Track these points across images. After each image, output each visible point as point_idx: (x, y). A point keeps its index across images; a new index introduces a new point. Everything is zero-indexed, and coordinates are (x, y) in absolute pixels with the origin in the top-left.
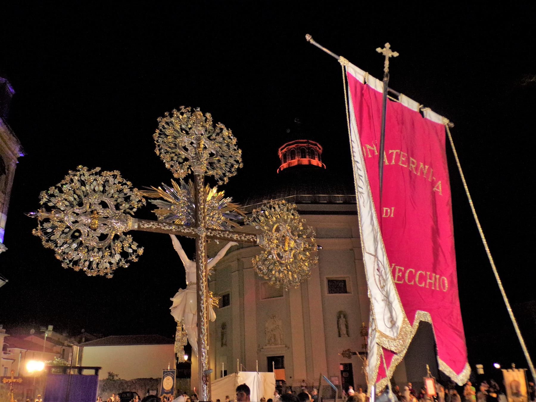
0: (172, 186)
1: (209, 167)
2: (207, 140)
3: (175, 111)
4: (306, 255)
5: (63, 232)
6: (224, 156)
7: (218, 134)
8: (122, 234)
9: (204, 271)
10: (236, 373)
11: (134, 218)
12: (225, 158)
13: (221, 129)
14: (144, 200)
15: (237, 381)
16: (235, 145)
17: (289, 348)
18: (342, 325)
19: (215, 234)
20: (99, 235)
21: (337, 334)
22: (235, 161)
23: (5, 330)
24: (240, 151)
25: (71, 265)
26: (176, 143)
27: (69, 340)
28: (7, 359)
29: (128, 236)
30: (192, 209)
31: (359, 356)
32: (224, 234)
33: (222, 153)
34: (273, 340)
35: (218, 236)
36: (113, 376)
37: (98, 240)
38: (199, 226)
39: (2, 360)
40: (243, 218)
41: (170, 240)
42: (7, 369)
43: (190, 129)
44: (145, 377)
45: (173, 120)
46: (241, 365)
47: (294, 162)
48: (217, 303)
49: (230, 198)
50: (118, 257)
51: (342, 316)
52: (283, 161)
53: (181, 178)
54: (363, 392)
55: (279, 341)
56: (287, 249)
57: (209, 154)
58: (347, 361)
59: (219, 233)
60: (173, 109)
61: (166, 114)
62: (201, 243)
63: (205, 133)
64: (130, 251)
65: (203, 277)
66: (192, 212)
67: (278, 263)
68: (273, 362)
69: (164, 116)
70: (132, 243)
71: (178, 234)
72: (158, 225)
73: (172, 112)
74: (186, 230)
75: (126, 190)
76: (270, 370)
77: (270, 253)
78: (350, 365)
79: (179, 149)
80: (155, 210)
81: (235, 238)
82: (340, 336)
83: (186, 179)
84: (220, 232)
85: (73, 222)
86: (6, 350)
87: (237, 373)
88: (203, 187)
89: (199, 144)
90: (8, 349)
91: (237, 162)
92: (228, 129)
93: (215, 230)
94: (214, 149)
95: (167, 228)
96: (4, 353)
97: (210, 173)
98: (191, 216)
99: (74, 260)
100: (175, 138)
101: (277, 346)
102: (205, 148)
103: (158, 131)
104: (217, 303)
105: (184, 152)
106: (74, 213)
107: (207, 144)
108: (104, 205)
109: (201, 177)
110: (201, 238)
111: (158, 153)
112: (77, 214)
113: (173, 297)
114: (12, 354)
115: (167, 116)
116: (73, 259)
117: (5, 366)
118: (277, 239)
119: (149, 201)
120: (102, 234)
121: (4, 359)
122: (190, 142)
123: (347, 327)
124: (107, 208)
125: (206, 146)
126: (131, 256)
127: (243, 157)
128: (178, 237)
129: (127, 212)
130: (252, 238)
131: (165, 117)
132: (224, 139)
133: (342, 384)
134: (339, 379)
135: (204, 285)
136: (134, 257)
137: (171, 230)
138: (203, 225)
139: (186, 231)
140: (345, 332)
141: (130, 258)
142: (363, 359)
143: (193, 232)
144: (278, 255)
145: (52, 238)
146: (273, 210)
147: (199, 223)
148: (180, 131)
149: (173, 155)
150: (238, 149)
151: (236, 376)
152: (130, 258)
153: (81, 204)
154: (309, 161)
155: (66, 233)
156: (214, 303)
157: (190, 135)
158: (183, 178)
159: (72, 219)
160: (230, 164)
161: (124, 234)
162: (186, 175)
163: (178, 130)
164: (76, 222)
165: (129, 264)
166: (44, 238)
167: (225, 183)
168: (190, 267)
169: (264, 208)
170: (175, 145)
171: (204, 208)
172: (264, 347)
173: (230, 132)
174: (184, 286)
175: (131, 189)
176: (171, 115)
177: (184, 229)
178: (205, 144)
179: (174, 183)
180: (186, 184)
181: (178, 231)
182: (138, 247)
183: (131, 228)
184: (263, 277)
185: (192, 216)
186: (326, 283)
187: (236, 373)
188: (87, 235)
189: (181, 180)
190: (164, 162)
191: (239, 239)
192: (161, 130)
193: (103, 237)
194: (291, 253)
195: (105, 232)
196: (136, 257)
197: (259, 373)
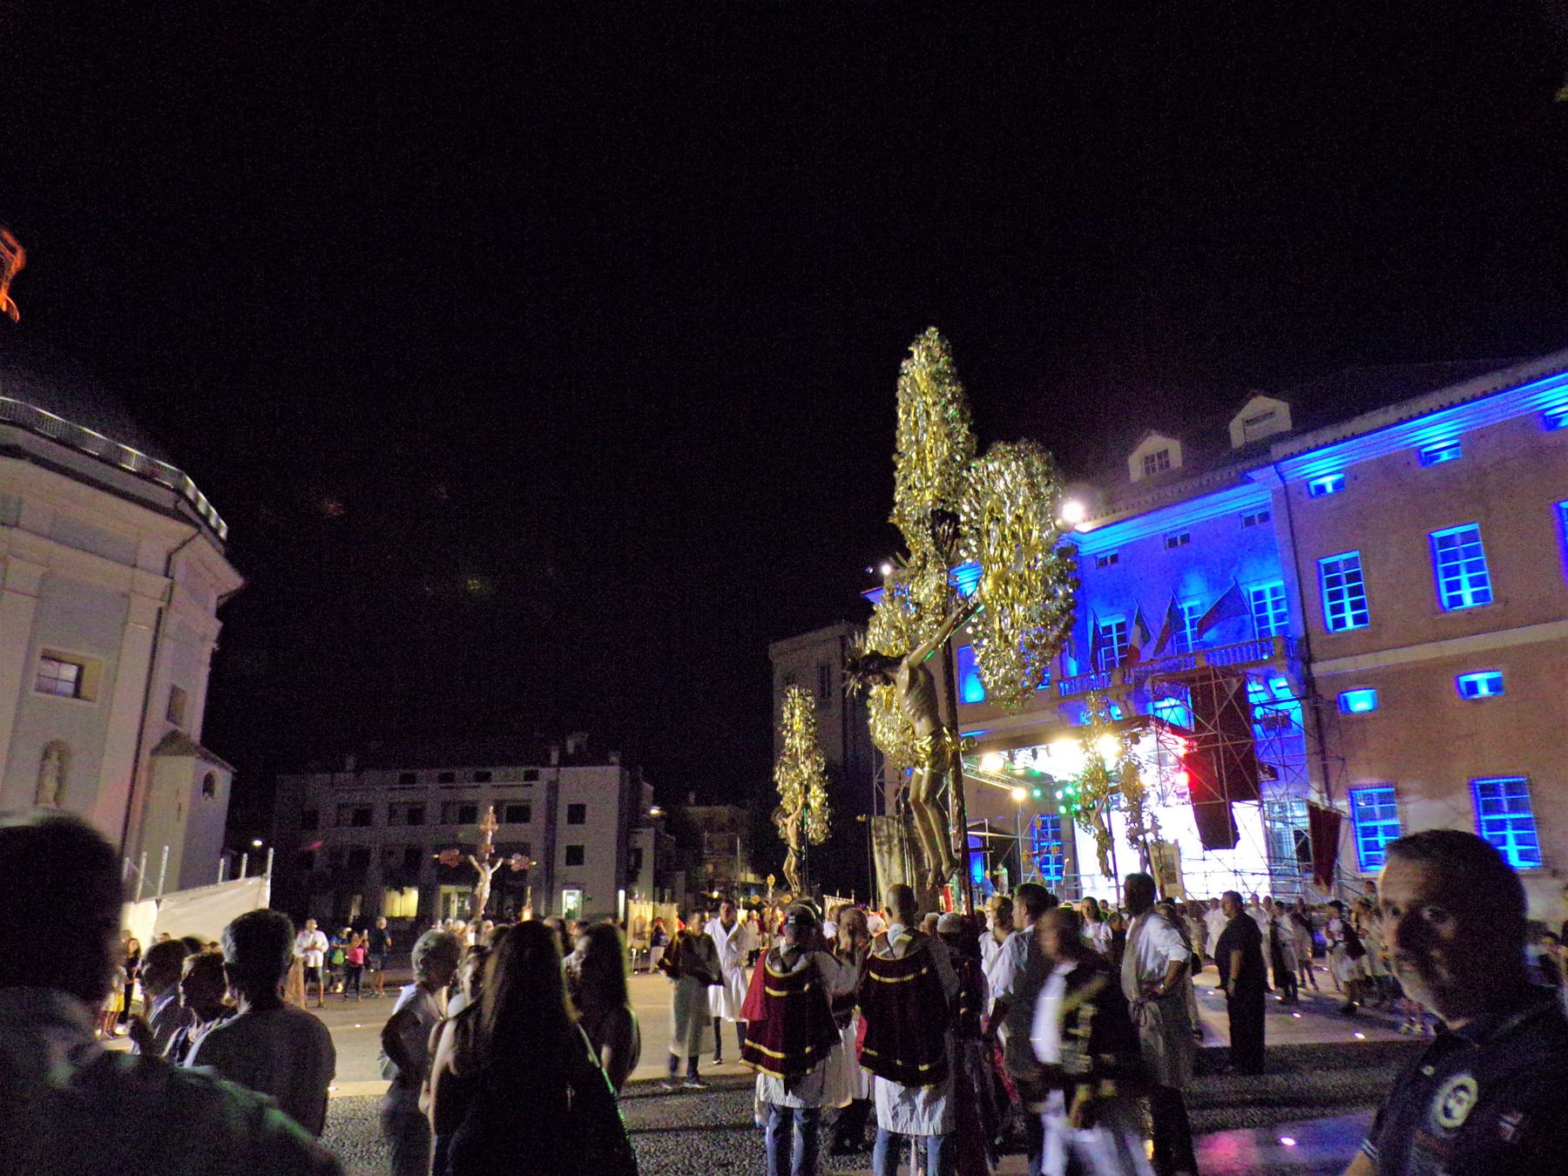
51: (55, 755)
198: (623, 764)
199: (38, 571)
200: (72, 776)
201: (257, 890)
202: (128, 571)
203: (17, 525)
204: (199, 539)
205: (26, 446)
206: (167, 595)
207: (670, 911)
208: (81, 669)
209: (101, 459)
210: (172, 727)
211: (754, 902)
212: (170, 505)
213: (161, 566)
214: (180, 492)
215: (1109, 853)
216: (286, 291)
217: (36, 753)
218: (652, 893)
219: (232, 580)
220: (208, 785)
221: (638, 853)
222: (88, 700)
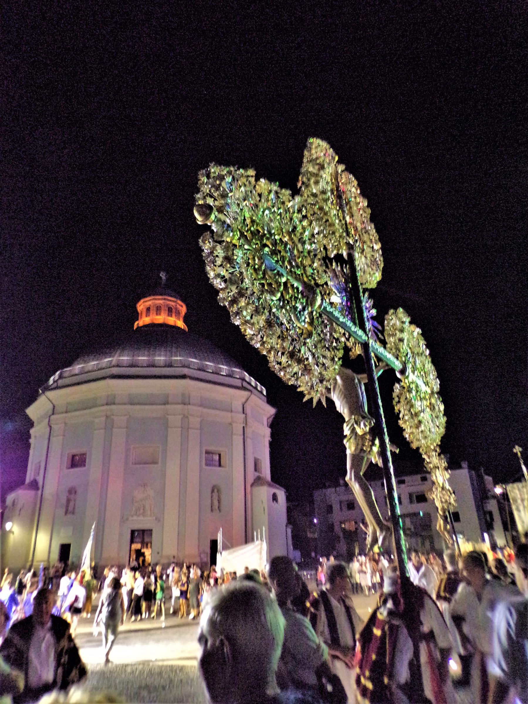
47: (159, 319)
51: (216, 490)
52: (144, 314)
55: (149, 513)
123: (219, 501)
154: (175, 322)
198: (471, 468)
199: (199, 419)
200: (223, 497)
202: (229, 414)
203: (189, 404)
204: (253, 397)
205: (187, 374)
208: (220, 455)
210: (257, 474)
211: (355, 566)
212: (240, 385)
214: (243, 380)
217: (210, 490)
218: (504, 535)
219: (271, 411)
220: (275, 498)
221: (491, 513)
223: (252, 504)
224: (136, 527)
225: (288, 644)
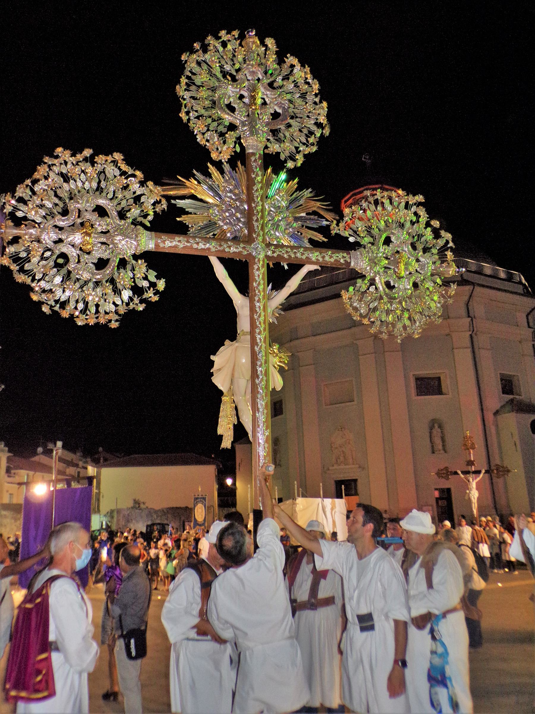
0: (208, 175)
1: (271, 138)
2: (269, 90)
3: (210, 39)
4: (435, 283)
5: (42, 258)
6: (297, 117)
7: (286, 78)
8: (132, 258)
9: (263, 314)
10: (293, 499)
11: (148, 232)
12: (297, 119)
13: (292, 66)
14: (164, 201)
15: (295, 509)
16: (316, 95)
17: (364, 469)
18: (436, 438)
19: (281, 253)
20: (96, 261)
21: (430, 450)
22: (316, 124)
23: (7, 449)
24: (325, 104)
25: (57, 308)
26: (215, 99)
27: (84, 460)
28: (11, 483)
29: (140, 261)
30: (242, 212)
31: (462, 476)
32: (295, 253)
33: (293, 111)
34: (342, 458)
35: (285, 256)
36: (139, 504)
37: (94, 268)
38: (255, 241)
39: (6, 484)
40: (328, 223)
41: (211, 267)
42: (12, 495)
43: (238, 71)
44: (178, 506)
45: (207, 56)
46: (300, 489)
48: (286, 362)
49: (307, 190)
50: (126, 294)
51: (436, 426)
53: (223, 161)
54: (467, 524)
55: (351, 461)
56: (403, 274)
57: (272, 114)
58: (445, 484)
59: (287, 252)
60: (208, 36)
61: (197, 45)
62: (258, 269)
63: (263, 77)
64: (145, 284)
65: (260, 323)
66: (242, 218)
67: (385, 299)
68: (343, 486)
69: (192, 51)
70: (147, 272)
71: (221, 255)
72: (188, 242)
73: (206, 42)
74: (232, 249)
75: (135, 187)
76: (339, 496)
77: (372, 282)
78: (449, 490)
79: (221, 108)
80: (183, 216)
81: (314, 259)
82: (433, 453)
83: (232, 162)
84: (289, 250)
85: (55, 242)
86: (10, 473)
87: (294, 499)
88: (260, 173)
89: (253, 98)
90: (13, 471)
91: (319, 125)
92: (303, 66)
93: (283, 246)
94: (280, 105)
95: (201, 246)
96: (9, 476)
97: (275, 148)
98: (241, 225)
99: (61, 300)
100: (214, 90)
101: (347, 467)
102: (264, 103)
103: (184, 80)
104: (286, 362)
105: (228, 114)
106: (56, 226)
107: (267, 97)
108: (101, 211)
109: (257, 156)
110: (256, 260)
111: (184, 117)
112: (61, 229)
113: (214, 354)
114: (17, 477)
115: (197, 51)
116: (59, 299)
117: (10, 492)
118: (387, 258)
119: (173, 201)
120: (100, 260)
121: (9, 483)
122: (238, 96)
124: (106, 217)
125: (267, 100)
126: (147, 292)
127: (328, 116)
128: (222, 260)
129: (138, 222)
130: (343, 257)
131: (195, 52)
132: (296, 86)
133: (438, 515)
134: (433, 508)
135: (262, 337)
136: (151, 295)
137: (209, 249)
138: (260, 239)
139: (233, 250)
140: (440, 447)
141: (146, 296)
142: (469, 481)
143: (243, 251)
144: (388, 285)
145: (27, 267)
146: (379, 208)
147: (254, 236)
148: (219, 75)
149: (209, 120)
150: (321, 102)
151: (294, 504)
152: (146, 296)
153: (65, 212)
155: (47, 259)
156: (280, 362)
157: (239, 81)
158: (227, 160)
159: (54, 236)
160: (305, 131)
161: (134, 259)
162: (231, 156)
163: (217, 74)
164: (60, 241)
165: (144, 305)
166: (14, 267)
167: (299, 165)
168: (242, 307)
169: (364, 204)
170: (214, 103)
171: (262, 211)
172: (331, 468)
173: (307, 69)
174: (233, 337)
175: (142, 184)
176: (205, 49)
177: (229, 247)
178: (265, 97)
179: (212, 169)
180: (233, 170)
181: (219, 251)
182: (158, 277)
183: (145, 248)
184: (361, 321)
185: (244, 223)
186: (412, 384)
187: (293, 499)
188: (77, 261)
189: (225, 163)
190: (195, 133)
191: (321, 259)
192: (188, 78)
193: (101, 264)
194: (410, 279)
195: (105, 256)
196: (155, 294)
197: (325, 499)
201: (291, 506)
206: (471, 328)
207: (166, 567)
209: (475, 272)
213: (463, 312)
215: (292, 588)
216: (239, 87)
222: (446, 394)
223: (506, 492)
224: (341, 477)
225: (458, 476)
